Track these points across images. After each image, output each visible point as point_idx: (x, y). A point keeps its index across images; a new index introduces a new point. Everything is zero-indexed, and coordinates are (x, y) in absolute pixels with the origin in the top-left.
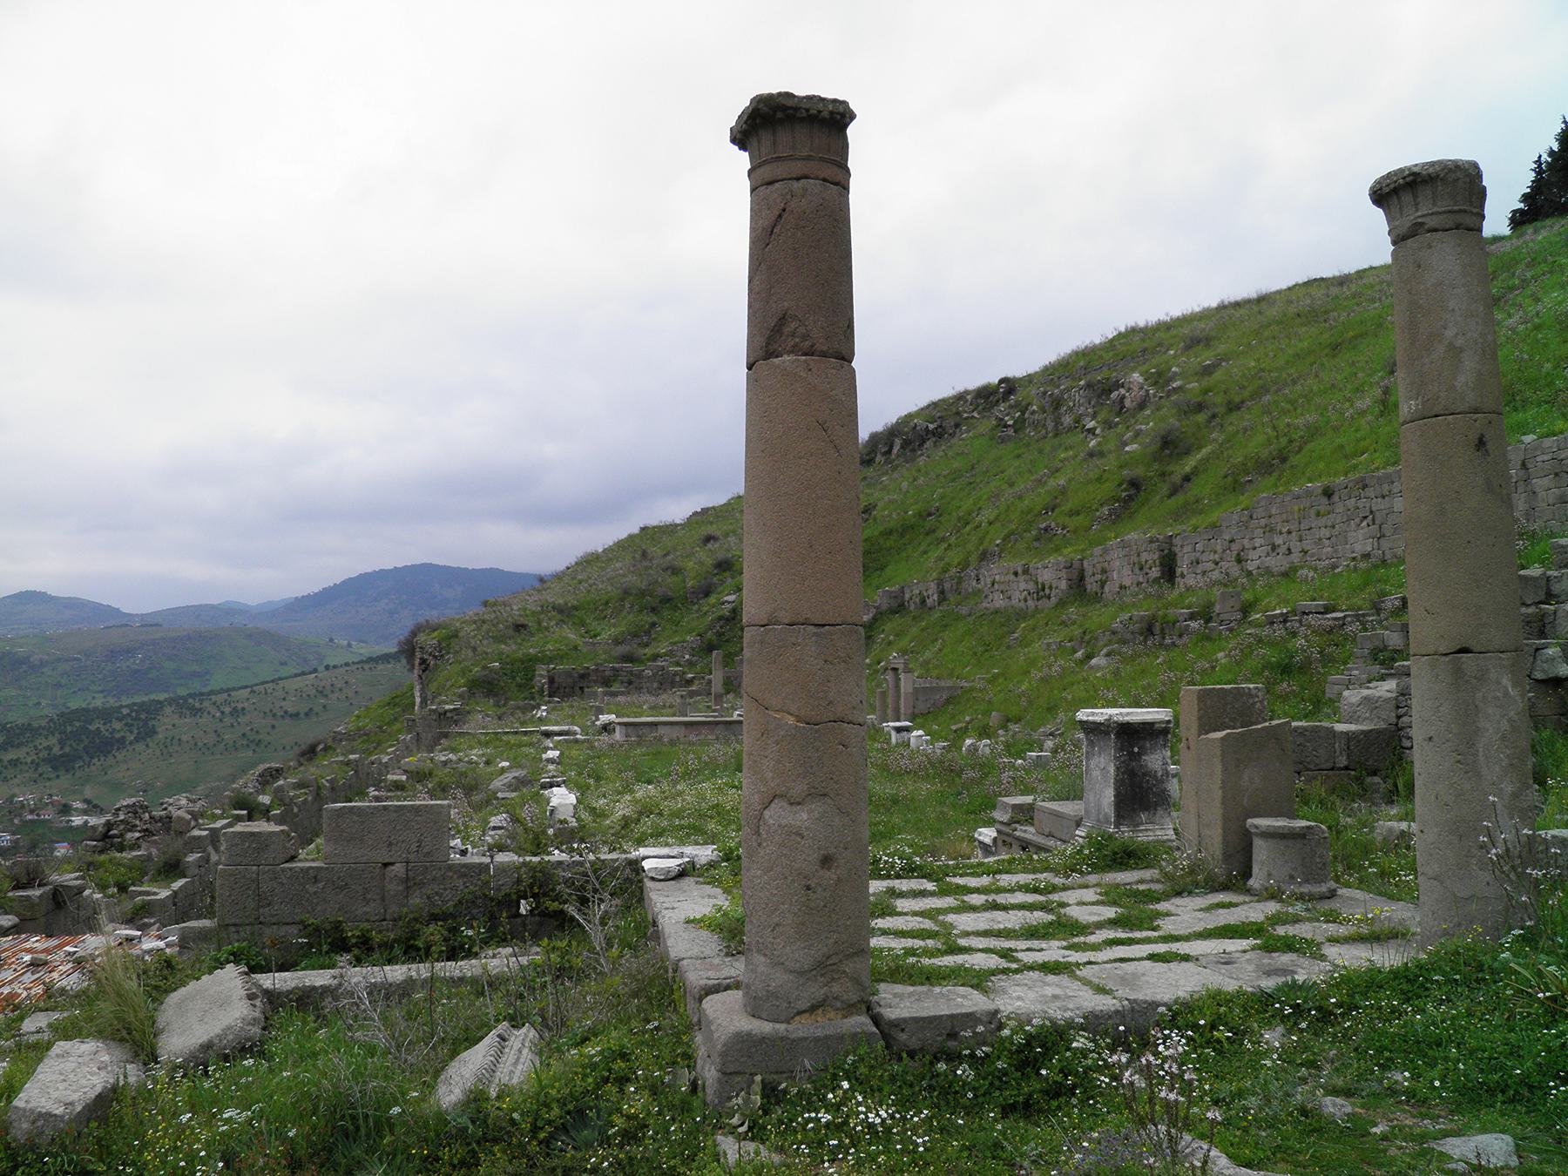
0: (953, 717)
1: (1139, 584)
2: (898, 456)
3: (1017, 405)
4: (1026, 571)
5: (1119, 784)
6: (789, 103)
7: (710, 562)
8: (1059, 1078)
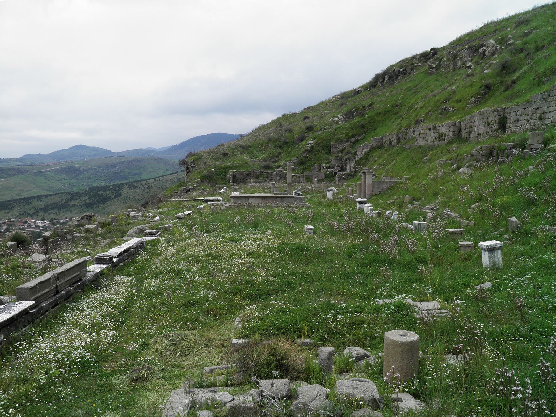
0: (390, 196)
1: (487, 132)
2: (387, 83)
3: (438, 58)
4: (434, 128)
7: (304, 127)
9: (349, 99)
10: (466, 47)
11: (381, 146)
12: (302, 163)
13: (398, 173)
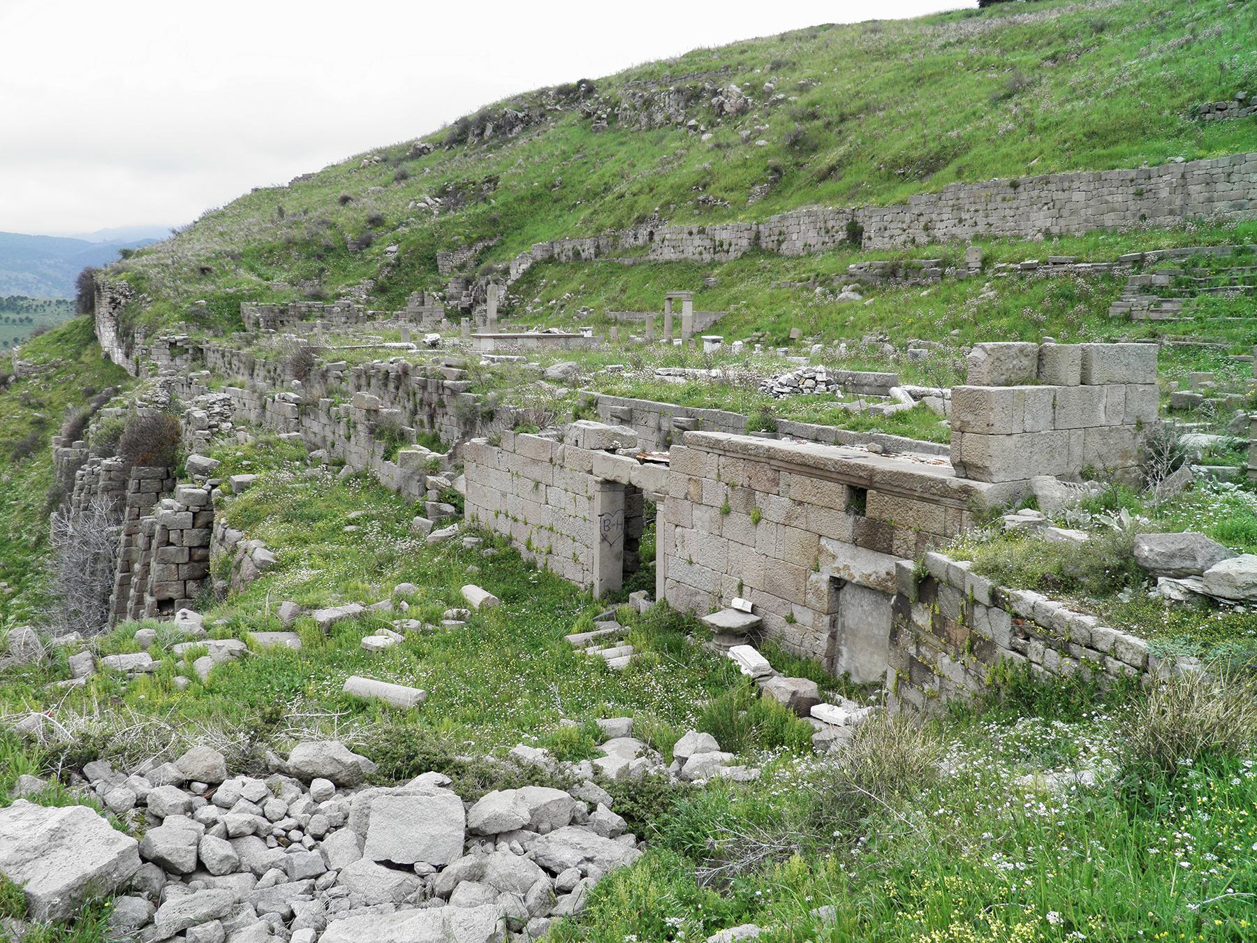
4: (702, 231)
10: (672, 88)
12: (381, 289)
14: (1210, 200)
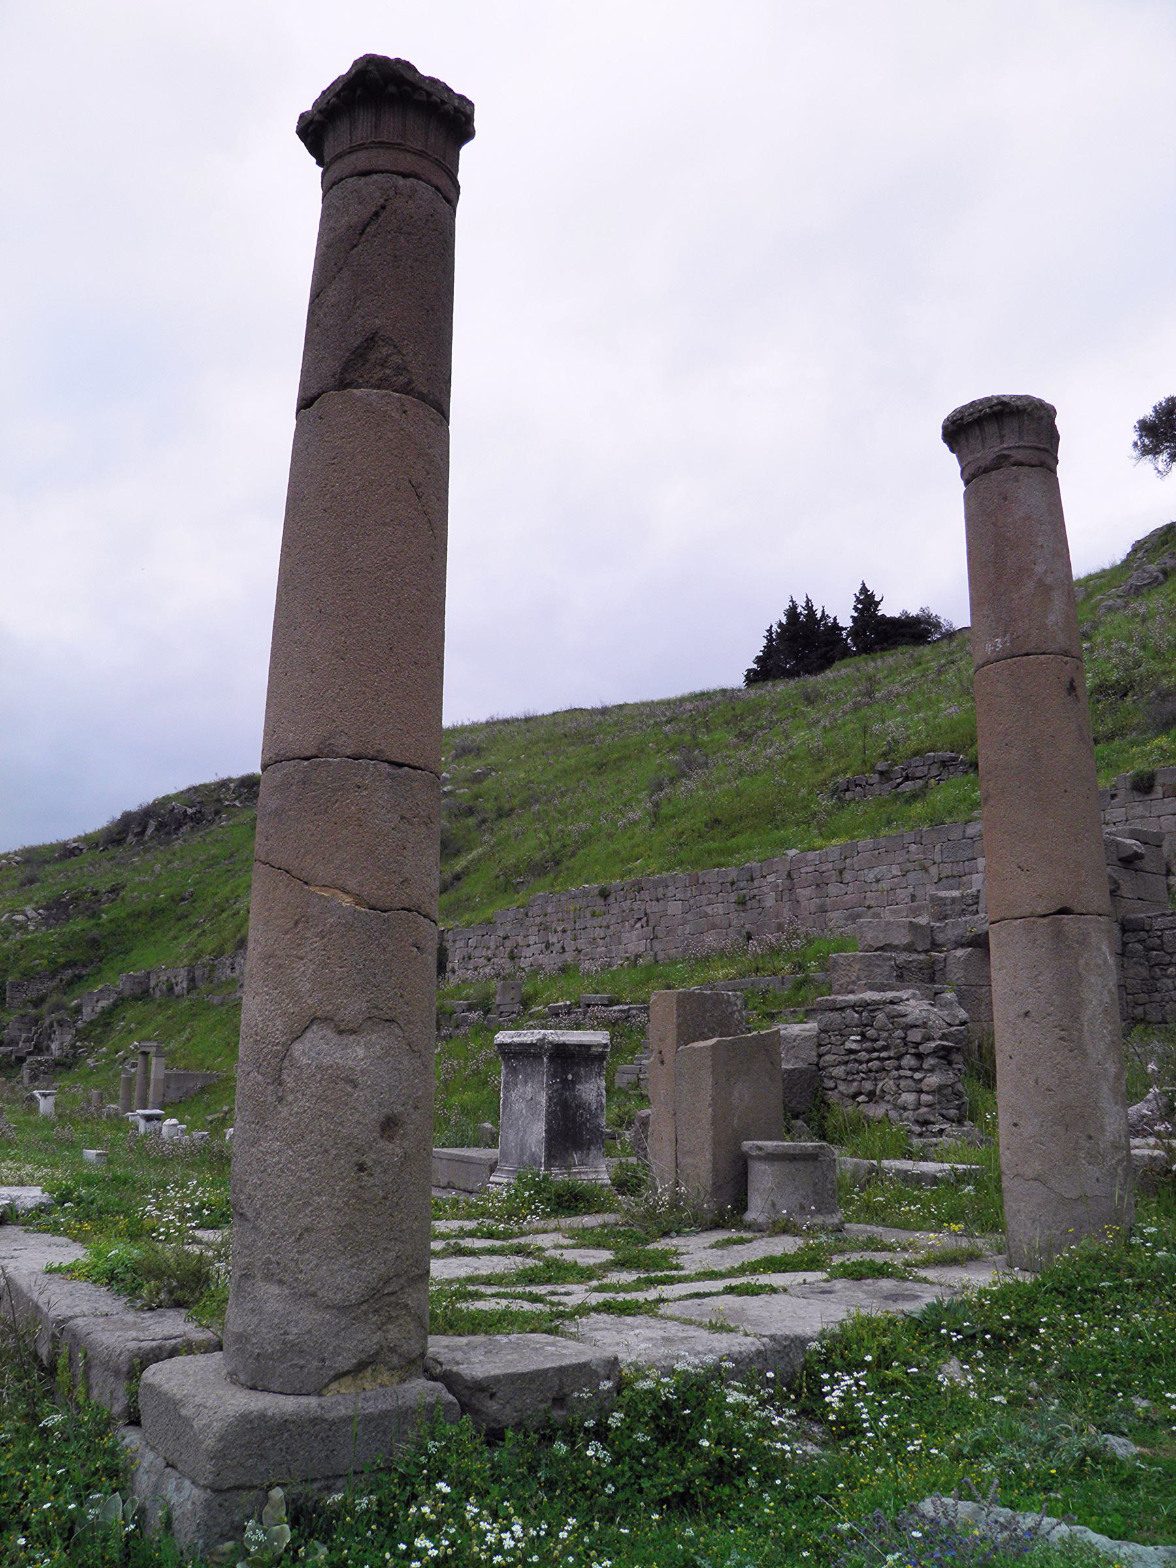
2: (151, 838)
5: (551, 1116)
6: (409, 76)
8: (720, 1451)
9: (49, 868)
11: (143, 994)
13: (203, 1060)
14: (823, 910)
